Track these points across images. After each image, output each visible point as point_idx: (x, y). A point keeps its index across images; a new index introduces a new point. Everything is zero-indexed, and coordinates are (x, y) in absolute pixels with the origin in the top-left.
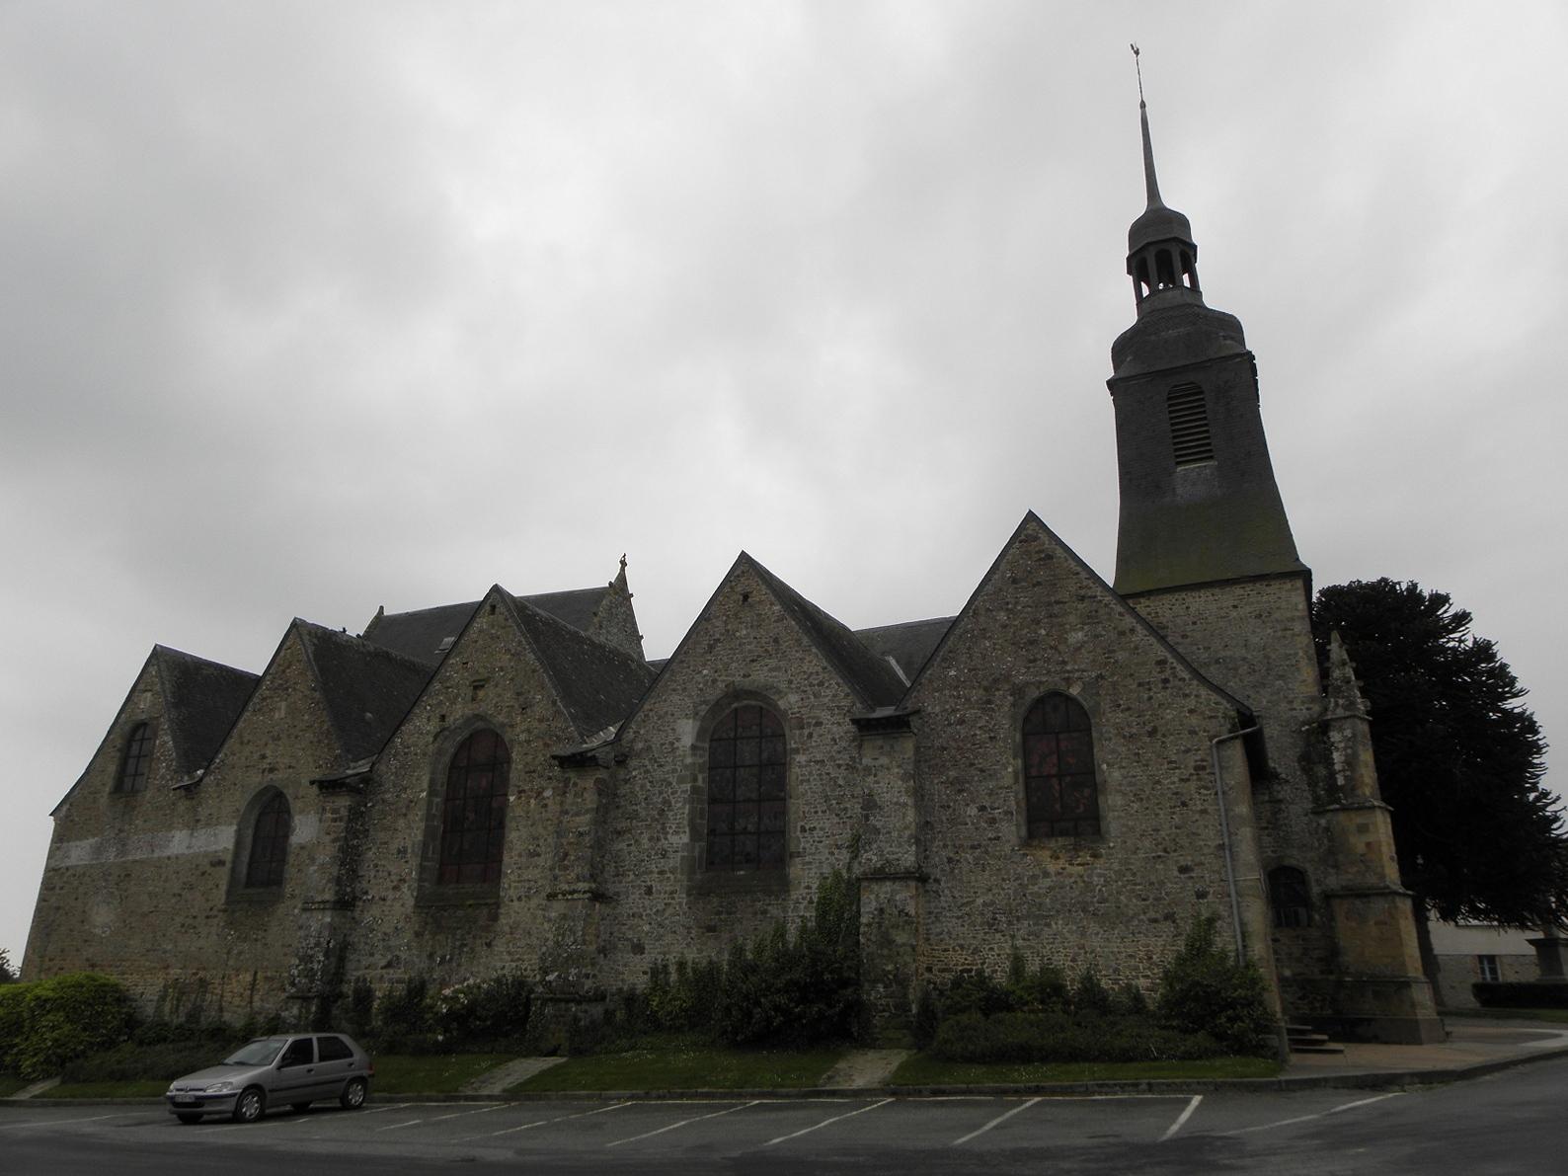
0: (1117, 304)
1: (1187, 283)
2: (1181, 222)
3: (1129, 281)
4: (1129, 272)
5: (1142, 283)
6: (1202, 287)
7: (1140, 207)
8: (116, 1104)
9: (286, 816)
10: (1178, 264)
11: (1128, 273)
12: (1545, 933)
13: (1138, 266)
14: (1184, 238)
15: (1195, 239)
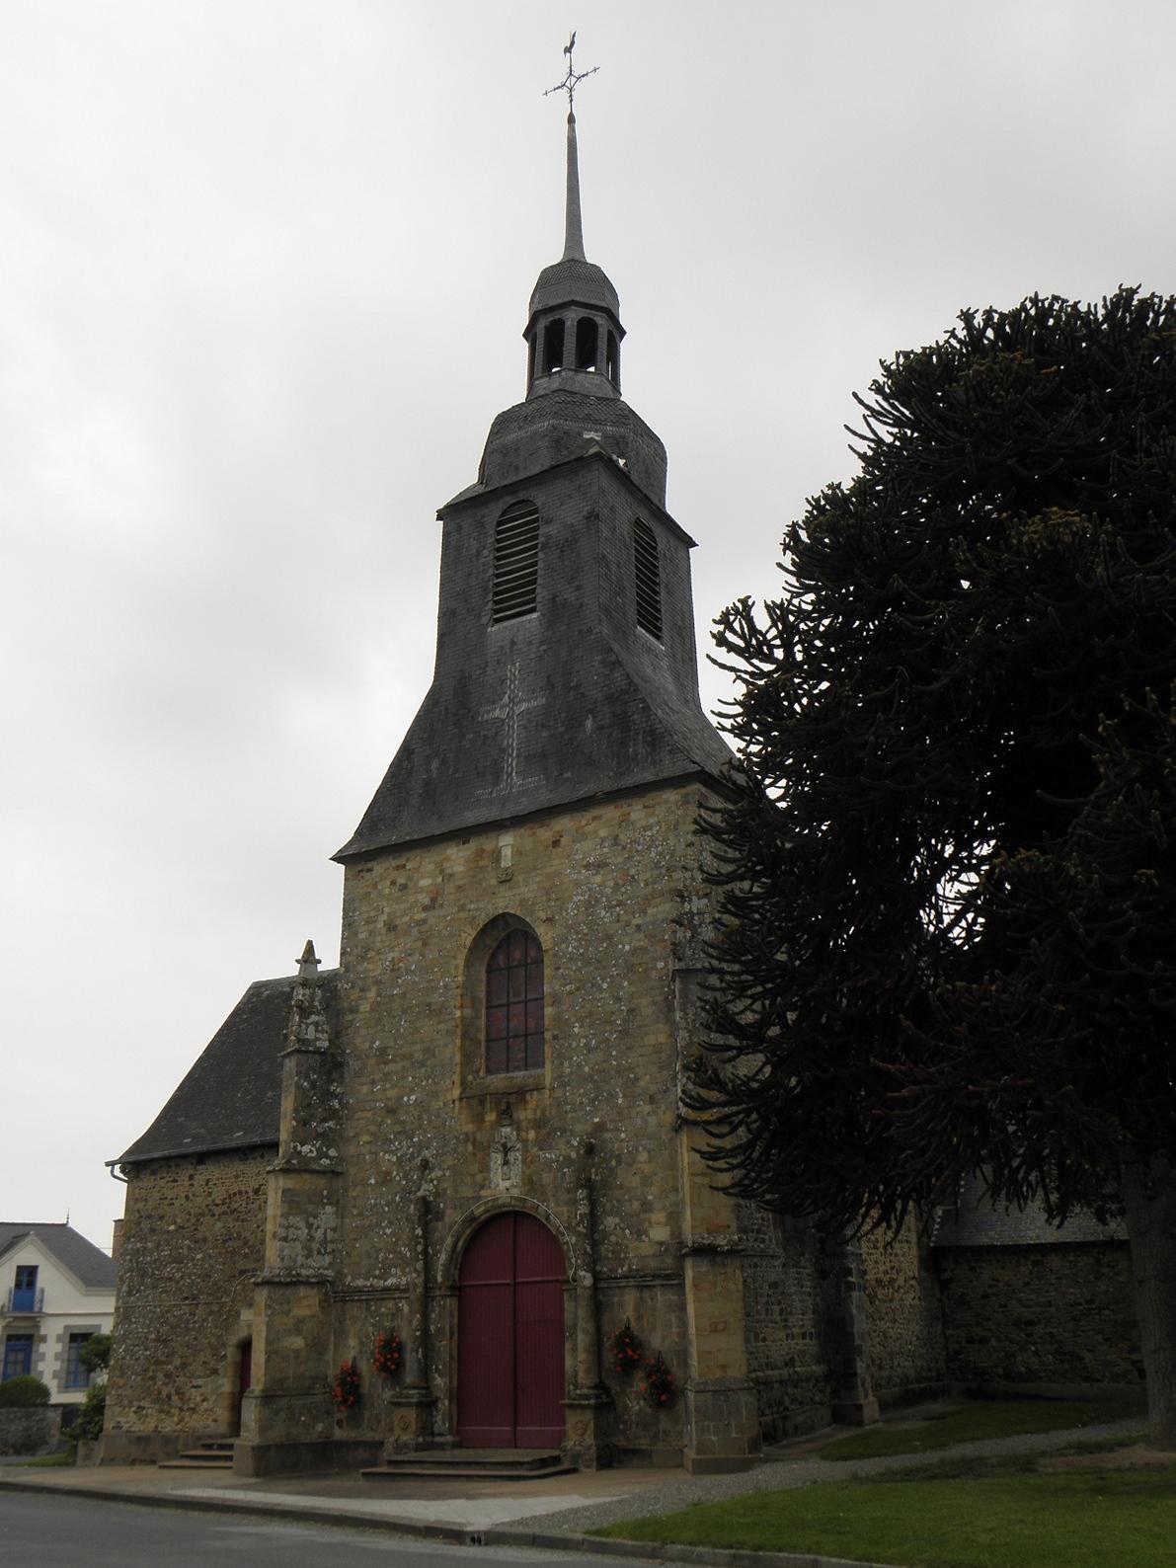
0: (505, 378)
7: (554, 253)
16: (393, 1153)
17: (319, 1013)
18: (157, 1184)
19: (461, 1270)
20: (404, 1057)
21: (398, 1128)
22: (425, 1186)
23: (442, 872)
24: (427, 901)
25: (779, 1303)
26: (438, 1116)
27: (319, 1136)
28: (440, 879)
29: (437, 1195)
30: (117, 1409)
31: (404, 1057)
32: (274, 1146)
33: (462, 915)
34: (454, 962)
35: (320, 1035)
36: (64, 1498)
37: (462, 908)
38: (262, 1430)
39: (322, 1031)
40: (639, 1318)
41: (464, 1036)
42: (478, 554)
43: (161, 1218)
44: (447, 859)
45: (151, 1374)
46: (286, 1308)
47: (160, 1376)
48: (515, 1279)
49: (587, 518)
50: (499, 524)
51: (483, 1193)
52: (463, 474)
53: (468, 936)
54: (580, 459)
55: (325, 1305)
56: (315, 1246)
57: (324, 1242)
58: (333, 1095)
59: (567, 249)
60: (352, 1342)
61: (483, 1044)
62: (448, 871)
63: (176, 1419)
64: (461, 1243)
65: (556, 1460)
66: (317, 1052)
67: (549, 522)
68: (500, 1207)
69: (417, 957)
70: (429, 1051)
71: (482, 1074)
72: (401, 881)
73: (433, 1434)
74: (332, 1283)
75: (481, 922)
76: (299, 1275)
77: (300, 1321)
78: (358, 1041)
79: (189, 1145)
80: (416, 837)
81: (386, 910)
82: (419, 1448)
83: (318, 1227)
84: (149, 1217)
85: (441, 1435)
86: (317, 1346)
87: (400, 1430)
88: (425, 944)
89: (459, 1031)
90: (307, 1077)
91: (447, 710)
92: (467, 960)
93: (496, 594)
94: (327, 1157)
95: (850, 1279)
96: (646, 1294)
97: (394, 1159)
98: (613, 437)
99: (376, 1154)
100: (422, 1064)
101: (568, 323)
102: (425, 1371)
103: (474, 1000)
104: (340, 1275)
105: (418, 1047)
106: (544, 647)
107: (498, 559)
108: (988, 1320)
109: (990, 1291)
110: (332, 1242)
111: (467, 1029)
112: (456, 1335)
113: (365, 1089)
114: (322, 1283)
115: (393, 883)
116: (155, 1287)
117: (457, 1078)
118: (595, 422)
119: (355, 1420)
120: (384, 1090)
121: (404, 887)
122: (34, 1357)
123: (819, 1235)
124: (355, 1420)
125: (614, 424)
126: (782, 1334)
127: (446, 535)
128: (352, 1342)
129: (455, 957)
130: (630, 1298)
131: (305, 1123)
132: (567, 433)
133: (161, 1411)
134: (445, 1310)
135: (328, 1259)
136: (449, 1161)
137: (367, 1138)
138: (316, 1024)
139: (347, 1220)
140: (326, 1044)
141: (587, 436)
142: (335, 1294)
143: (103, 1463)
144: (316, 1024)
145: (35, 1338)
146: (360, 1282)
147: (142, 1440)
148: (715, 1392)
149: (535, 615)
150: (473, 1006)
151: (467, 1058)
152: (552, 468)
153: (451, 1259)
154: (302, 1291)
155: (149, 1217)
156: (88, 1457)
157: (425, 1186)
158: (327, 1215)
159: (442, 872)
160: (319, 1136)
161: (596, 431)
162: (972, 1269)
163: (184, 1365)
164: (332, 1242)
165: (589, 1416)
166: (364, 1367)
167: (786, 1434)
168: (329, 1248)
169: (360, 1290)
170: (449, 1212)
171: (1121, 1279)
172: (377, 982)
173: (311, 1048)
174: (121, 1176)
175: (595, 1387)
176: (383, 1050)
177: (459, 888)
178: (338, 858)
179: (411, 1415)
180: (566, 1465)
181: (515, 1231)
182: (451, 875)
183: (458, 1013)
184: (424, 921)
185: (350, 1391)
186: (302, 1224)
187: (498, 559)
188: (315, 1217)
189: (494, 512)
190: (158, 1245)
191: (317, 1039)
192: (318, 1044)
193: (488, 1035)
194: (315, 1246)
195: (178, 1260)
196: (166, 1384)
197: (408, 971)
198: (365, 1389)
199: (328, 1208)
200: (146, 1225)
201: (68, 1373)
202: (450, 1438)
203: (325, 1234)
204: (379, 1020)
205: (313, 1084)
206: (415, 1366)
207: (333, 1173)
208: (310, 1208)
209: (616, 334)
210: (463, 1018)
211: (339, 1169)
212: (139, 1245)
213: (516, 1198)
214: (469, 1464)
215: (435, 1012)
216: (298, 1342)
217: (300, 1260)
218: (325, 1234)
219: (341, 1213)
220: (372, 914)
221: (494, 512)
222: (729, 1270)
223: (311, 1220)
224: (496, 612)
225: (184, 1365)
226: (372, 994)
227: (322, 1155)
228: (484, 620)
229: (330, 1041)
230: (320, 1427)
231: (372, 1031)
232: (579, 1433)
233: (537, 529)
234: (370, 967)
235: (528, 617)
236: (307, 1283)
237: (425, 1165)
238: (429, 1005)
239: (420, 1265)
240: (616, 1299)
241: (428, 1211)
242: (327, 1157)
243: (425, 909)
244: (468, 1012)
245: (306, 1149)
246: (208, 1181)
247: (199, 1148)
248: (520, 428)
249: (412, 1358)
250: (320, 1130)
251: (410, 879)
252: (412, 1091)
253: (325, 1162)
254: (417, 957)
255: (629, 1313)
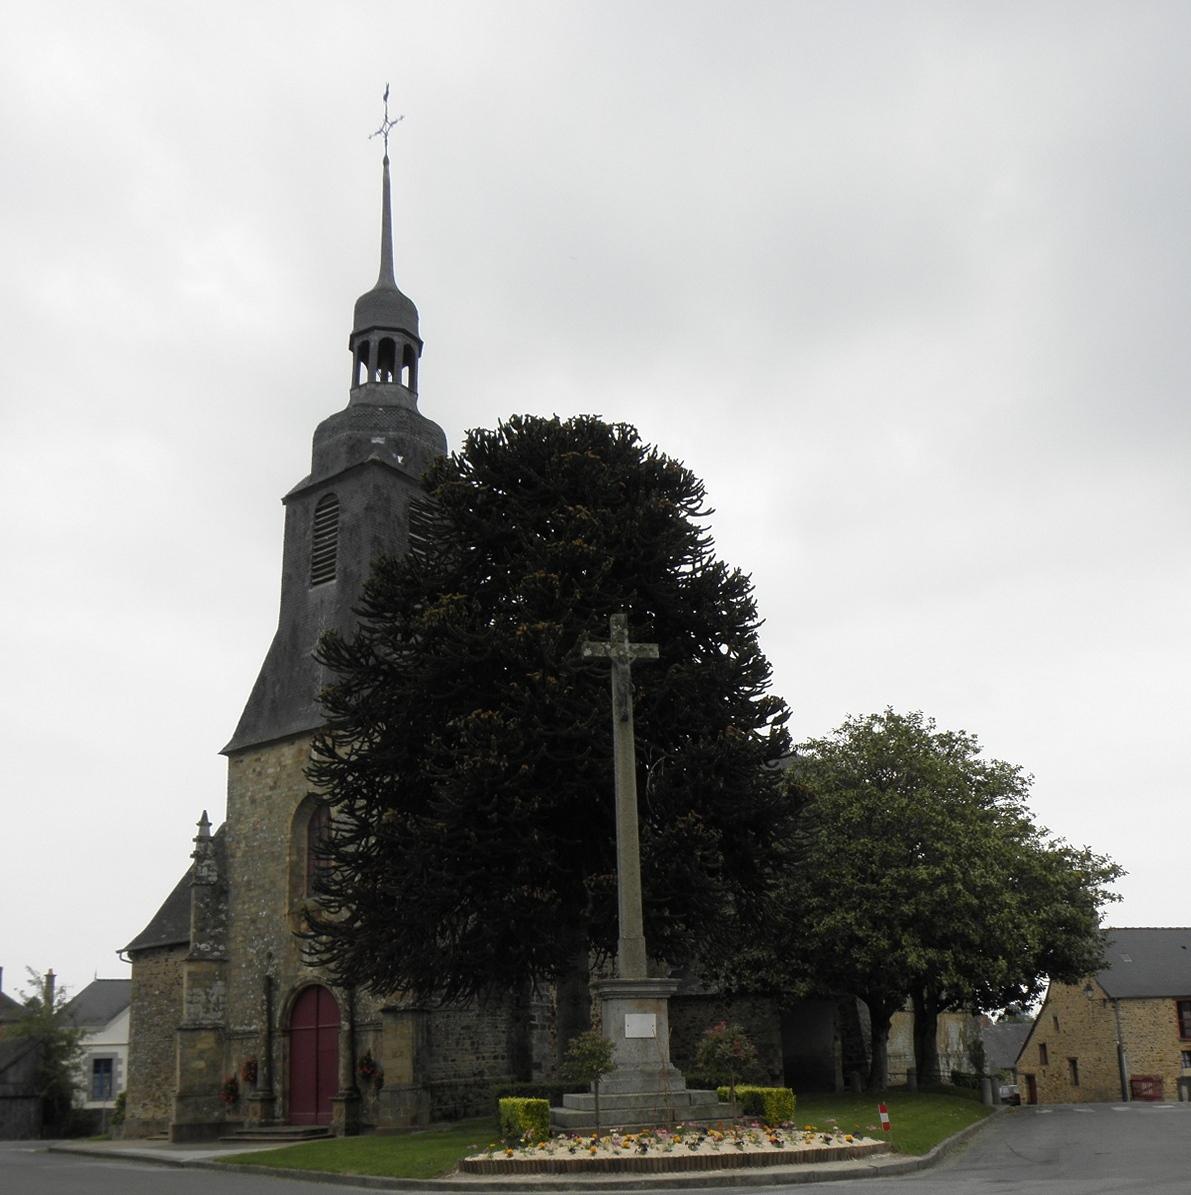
0: (330, 382)
1: (405, 382)
2: (408, 309)
3: (349, 357)
4: (351, 348)
5: (362, 364)
6: (419, 390)
7: (369, 282)
8: (230, 1170)
9: (644, 859)
10: (399, 357)
11: (350, 349)
12: (365, 385)
13: (360, 348)
14: (411, 332)
15: (422, 335)
16: (254, 948)
17: (210, 859)
18: (148, 963)
19: (291, 1020)
20: (260, 887)
21: (257, 932)
22: (271, 969)
23: (280, 764)
24: (272, 784)
25: (471, 1038)
26: (277, 925)
27: (212, 937)
28: (279, 769)
29: (277, 974)
30: (132, 1106)
31: (260, 887)
32: (187, 944)
33: (290, 793)
34: (286, 824)
35: (210, 873)
36: (73, 1156)
37: (290, 789)
38: (178, 1116)
39: (213, 871)
40: (375, 1050)
41: (292, 873)
42: (305, 533)
43: (151, 986)
44: (283, 755)
45: (148, 1084)
46: (192, 1044)
47: (154, 1085)
48: (318, 1024)
49: (366, 509)
50: (318, 510)
51: (300, 973)
52: (299, 467)
53: (293, 807)
54: (362, 464)
55: (219, 1041)
56: (211, 1006)
57: (217, 1004)
58: (221, 911)
59: (382, 276)
60: (235, 1064)
61: (306, 878)
62: (283, 764)
63: (163, 1111)
64: (289, 1005)
65: (325, 1131)
66: (208, 884)
67: (344, 511)
68: (309, 981)
69: (266, 821)
70: (273, 883)
71: (304, 897)
72: (258, 769)
73: (274, 1118)
74: (223, 1029)
75: (300, 800)
76: (201, 1024)
77: (202, 1052)
78: (236, 876)
79: (164, 940)
80: (264, 740)
81: (251, 789)
82: (261, 1125)
83: (212, 995)
84: (145, 985)
85: (278, 1118)
86: (214, 1067)
87: (252, 1114)
88: (270, 812)
89: (288, 871)
90: (202, 901)
91: (285, 648)
92: (293, 823)
93: (314, 564)
94: (218, 950)
95: (532, 1022)
96: (379, 1035)
97: (255, 952)
98: (394, 440)
99: (245, 949)
100: (269, 891)
101: (372, 344)
102: (269, 1081)
103: (299, 851)
104: (228, 1024)
105: (267, 880)
106: (339, 606)
107: (317, 537)
108: (688, 1044)
109: (691, 1025)
110: (223, 1003)
111: (293, 869)
112: (288, 1060)
113: (240, 907)
114: (215, 1028)
115: (254, 771)
116: (149, 1030)
117: (287, 901)
118: (381, 430)
119: (236, 1110)
120: (249, 908)
121: (260, 774)
122: (114, 1075)
123: (516, 995)
124: (236, 1110)
125: (395, 430)
126: (474, 1058)
127: (287, 511)
128: (235, 1064)
129: (286, 821)
130: (371, 1036)
131: (202, 930)
132: (359, 441)
133: (156, 1106)
134: (280, 1044)
135: (220, 1014)
136: (283, 954)
137: (240, 939)
138: (209, 866)
139: (231, 990)
140: (215, 879)
141: (374, 441)
142: (224, 1035)
143: (125, 1138)
144: (209, 866)
145: (114, 1062)
146: (238, 1028)
147: (146, 1123)
148: (392, 1092)
149: (334, 582)
150: (298, 853)
151: (294, 888)
152: (347, 470)
153: (283, 1014)
154: (203, 1034)
155: (145, 985)
156: (119, 1134)
157: (271, 969)
158: (218, 987)
159: (280, 764)
160: (212, 937)
161: (381, 436)
162: (681, 1010)
163: (167, 1079)
164: (223, 1003)
165: (343, 1106)
166: (240, 1078)
167: (466, 1115)
168: (221, 1007)
169: (237, 1033)
170: (282, 985)
171: (765, 1016)
172: (245, 838)
173: (204, 882)
174: (128, 959)
175: (350, 1089)
176: (249, 882)
177: (289, 775)
178: (222, 753)
179: (258, 1106)
180: (329, 1134)
181: (318, 999)
182: (285, 766)
183: (288, 859)
184: (270, 797)
185: (232, 1093)
186: (202, 993)
187: (317, 537)
188: (211, 988)
189: (313, 501)
190: (150, 1003)
191: (209, 876)
192: (210, 879)
193: (308, 872)
194: (211, 1006)
195: (160, 1013)
196: (157, 1090)
197: (262, 831)
198: (241, 1092)
199: (220, 983)
200: (143, 991)
201: (94, 1087)
202: (282, 1120)
203: (218, 999)
204: (246, 863)
205: (207, 905)
206: (262, 1078)
207: (222, 961)
208: (207, 983)
209: (415, 346)
210: (291, 862)
211: (226, 958)
212: (140, 1004)
213: (316, 977)
214: (287, 1133)
215: (275, 858)
216: (201, 1064)
217: (201, 1015)
218: (218, 999)
219: (227, 986)
220: (243, 791)
221: (313, 501)
222: (405, 1021)
223: (208, 990)
224: (314, 577)
225: (167, 1079)
226: (243, 845)
227: (214, 949)
228: (307, 584)
229: (218, 876)
230: (216, 1114)
231: (243, 869)
232: (338, 1116)
233: (337, 516)
234: (242, 827)
235: (330, 583)
236: (205, 1029)
237: (270, 956)
238: (273, 853)
239: (264, 1018)
240: (364, 1038)
241: (270, 984)
242: (218, 950)
243: (272, 788)
244: (294, 858)
245: (203, 946)
246: (176, 963)
247: (170, 941)
248: (330, 436)
249: (261, 1073)
250: (212, 934)
251: (262, 768)
252: (264, 909)
253: (216, 953)
254: (266, 821)
255: (370, 1046)
